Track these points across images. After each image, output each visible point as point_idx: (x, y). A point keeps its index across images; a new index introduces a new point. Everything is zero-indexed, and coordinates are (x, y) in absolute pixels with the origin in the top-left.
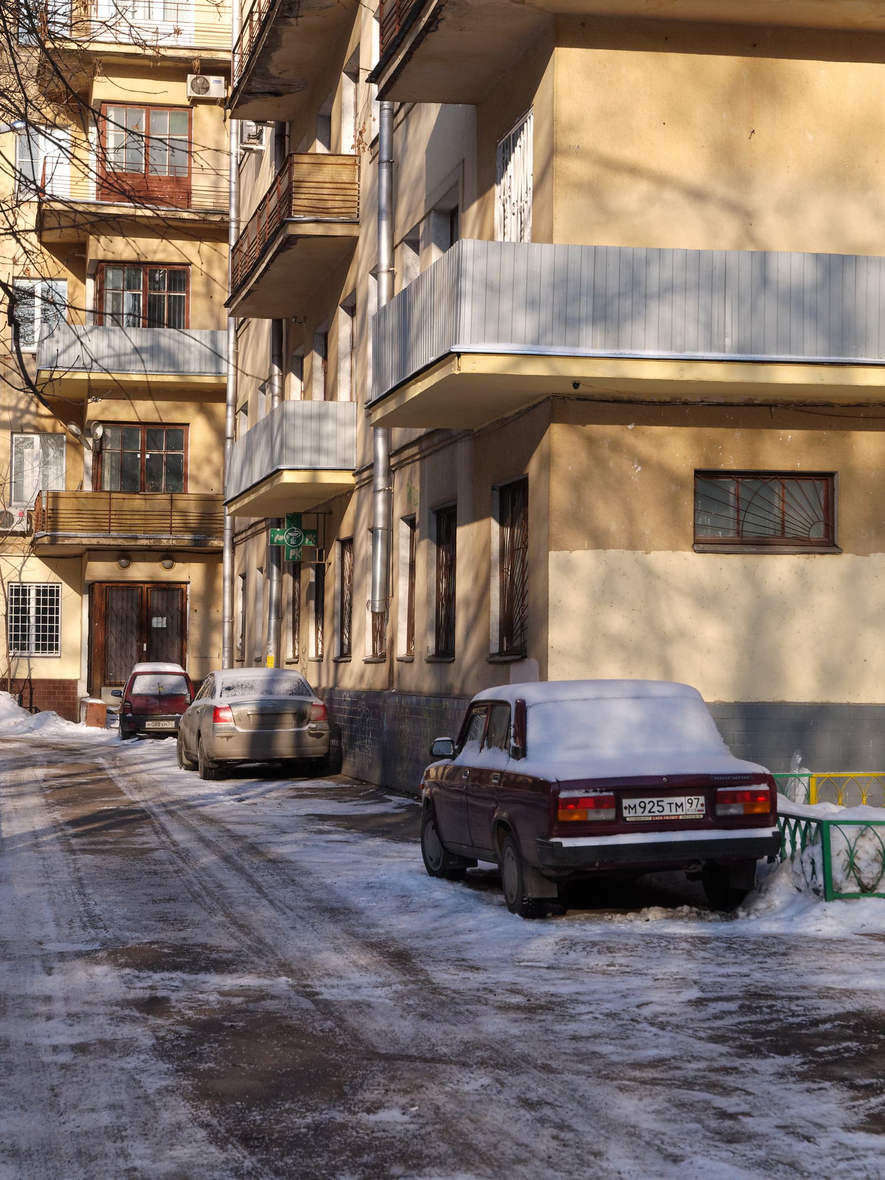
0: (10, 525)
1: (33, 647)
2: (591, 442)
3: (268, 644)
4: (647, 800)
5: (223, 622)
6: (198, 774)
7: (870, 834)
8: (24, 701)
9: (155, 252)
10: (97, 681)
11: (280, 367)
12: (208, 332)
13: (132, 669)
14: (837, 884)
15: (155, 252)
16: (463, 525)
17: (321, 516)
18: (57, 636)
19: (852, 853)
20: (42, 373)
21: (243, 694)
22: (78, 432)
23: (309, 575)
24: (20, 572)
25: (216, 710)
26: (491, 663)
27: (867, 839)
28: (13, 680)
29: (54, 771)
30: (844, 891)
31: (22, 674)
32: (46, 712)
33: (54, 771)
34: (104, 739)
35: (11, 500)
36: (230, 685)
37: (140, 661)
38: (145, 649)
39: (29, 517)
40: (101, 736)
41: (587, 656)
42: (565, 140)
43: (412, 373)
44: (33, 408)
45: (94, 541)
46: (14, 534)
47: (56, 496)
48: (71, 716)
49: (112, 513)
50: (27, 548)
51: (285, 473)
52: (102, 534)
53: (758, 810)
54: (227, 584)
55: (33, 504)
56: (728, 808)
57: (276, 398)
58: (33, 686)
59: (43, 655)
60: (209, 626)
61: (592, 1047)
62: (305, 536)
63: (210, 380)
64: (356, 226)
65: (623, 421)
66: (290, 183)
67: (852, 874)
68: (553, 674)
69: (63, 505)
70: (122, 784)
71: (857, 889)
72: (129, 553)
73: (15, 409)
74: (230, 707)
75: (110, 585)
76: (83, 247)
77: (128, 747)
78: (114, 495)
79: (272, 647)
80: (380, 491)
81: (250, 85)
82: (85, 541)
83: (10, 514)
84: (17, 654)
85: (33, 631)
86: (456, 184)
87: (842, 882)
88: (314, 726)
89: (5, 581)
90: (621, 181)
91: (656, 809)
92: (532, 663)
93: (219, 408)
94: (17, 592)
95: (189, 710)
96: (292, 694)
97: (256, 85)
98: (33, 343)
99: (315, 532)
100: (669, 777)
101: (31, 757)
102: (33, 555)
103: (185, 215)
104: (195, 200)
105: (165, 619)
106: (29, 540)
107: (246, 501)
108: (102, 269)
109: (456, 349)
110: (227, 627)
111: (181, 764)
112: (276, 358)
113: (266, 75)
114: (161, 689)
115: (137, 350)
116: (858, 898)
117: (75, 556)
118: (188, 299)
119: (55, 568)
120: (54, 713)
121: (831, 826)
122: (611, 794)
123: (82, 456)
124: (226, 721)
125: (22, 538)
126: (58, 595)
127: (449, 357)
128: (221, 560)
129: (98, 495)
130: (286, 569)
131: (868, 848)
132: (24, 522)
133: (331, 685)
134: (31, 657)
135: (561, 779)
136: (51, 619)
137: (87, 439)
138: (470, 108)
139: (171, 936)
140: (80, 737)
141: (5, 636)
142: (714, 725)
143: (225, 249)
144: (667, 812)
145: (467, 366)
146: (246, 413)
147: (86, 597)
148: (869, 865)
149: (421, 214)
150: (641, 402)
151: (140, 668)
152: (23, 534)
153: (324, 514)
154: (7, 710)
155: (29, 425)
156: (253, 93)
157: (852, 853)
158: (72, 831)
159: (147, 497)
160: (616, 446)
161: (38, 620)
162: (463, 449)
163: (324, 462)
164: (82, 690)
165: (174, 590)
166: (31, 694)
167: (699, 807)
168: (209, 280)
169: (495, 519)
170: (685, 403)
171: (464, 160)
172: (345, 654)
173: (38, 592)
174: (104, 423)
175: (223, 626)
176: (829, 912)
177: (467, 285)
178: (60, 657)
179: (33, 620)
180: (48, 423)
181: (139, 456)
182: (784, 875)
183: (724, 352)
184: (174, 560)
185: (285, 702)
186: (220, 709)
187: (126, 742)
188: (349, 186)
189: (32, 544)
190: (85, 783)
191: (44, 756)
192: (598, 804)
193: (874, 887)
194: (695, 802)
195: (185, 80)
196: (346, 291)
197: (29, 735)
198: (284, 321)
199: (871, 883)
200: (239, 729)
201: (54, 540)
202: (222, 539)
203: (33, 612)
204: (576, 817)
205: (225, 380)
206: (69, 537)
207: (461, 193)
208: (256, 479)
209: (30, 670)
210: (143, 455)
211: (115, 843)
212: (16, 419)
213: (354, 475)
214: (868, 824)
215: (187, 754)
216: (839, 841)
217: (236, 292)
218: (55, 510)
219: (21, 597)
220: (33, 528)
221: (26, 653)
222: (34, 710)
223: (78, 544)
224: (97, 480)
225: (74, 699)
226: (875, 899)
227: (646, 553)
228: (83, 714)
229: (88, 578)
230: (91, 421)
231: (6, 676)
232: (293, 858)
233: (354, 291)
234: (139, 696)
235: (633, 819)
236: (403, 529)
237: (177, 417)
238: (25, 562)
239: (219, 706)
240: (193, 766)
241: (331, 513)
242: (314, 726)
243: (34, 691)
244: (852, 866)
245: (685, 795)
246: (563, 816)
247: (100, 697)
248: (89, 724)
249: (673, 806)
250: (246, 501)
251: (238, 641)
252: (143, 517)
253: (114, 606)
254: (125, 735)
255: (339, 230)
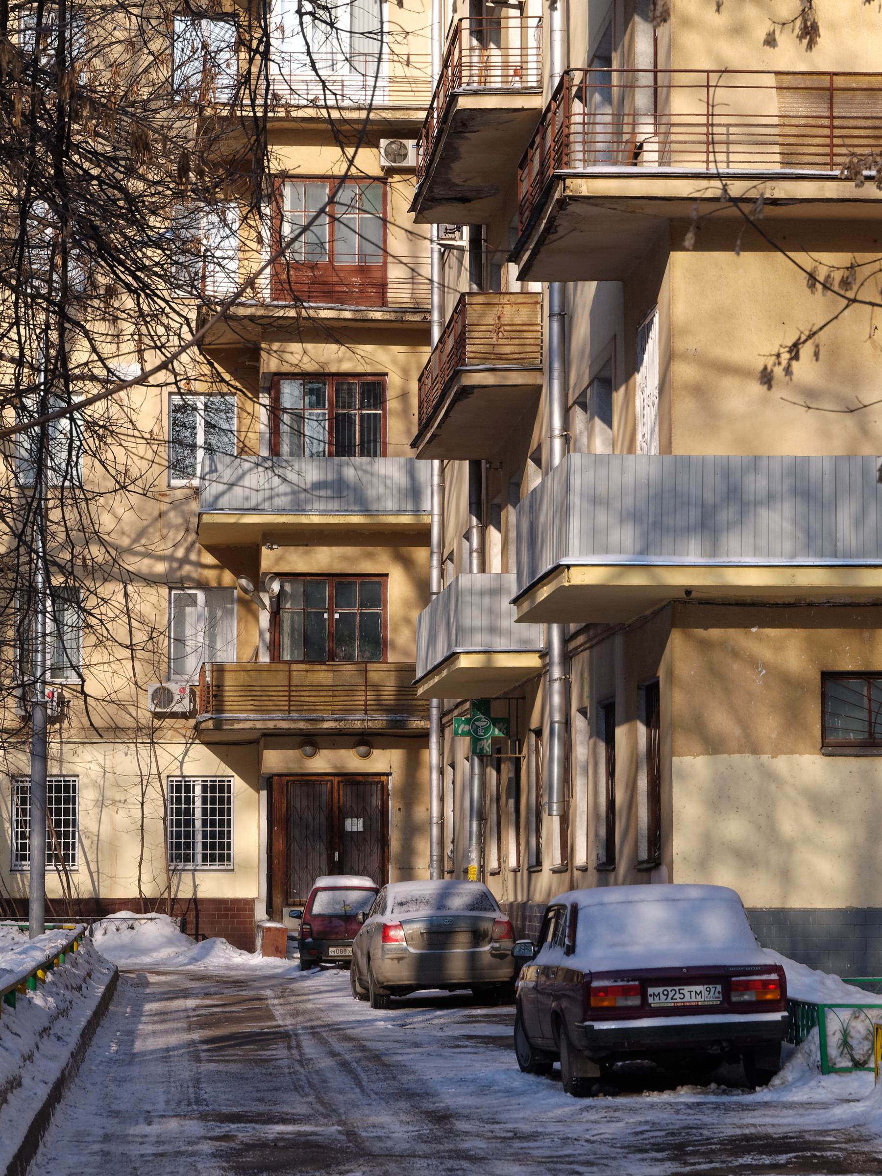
0: (169, 705)
1: (199, 857)
2: (705, 645)
3: (470, 851)
4: (669, 989)
5: (431, 823)
6: (369, 1004)
7: (862, 1016)
8: (188, 926)
9: (340, 361)
10: (278, 900)
11: (479, 518)
12: (402, 460)
13: (314, 881)
14: (831, 1059)
15: (340, 361)
16: (619, 725)
17: (513, 702)
18: (229, 843)
19: (845, 1033)
20: (204, 516)
21: (417, 910)
22: (251, 587)
23: (507, 770)
24: (182, 763)
25: (385, 928)
26: (639, 870)
27: (859, 1020)
28: (175, 901)
29: (208, 1002)
30: (838, 1066)
31: (185, 892)
32: (214, 939)
33: (208, 1002)
34: (279, 971)
35: (169, 673)
36: (404, 900)
37: (321, 874)
38: (337, 859)
39: (193, 693)
40: (276, 967)
41: (703, 863)
42: (680, 345)
43: (539, 576)
44: (193, 557)
45: (271, 725)
46: (174, 715)
47: (219, 670)
48: (245, 944)
49: (293, 688)
50: (189, 733)
51: (462, 656)
52: (279, 715)
53: (769, 997)
54: (435, 776)
55: (197, 677)
56: (743, 995)
57: (475, 555)
58: (199, 907)
59: (212, 867)
60: (411, 830)
61: (527, 1151)
62: (494, 726)
63: (406, 519)
64: (538, 374)
65: (745, 624)
66: (464, 326)
67: (846, 1051)
68: (678, 879)
69: (229, 680)
70: (278, 1012)
71: (850, 1064)
72: (314, 738)
73: (171, 558)
74: (401, 925)
75: (291, 778)
76: (255, 353)
77: (304, 978)
78: (294, 667)
79: (474, 855)
80: (556, 680)
81: (432, 192)
82: (259, 725)
83: (169, 690)
84: (180, 867)
85: (199, 838)
86: (610, 358)
87: (836, 1057)
88: (497, 945)
89: (163, 776)
90: (729, 383)
91: (677, 996)
92: (664, 869)
93: (420, 554)
94: (178, 789)
95: (363, 929)
96: (473, 909)
97: (439, 192)
98: (194, 475)
99: (506, 721)
100: (688, 968)
101: (187, 989)
102: (197, 741)
103: (378, 315)
104: (391, 295)
105: (361, 820)
106: (192, 722)
107: (431, 683)
108: (278, 384)
109: (565, 561)
110: (435, 830)
111: (356, 994)
112: (474, 506)
113: (448, 184)
114: (348, 908)
115: (318, 485)
116: (851, 1072)
117: (250, 742)
118: (385, 418)
119: (226, 759)
120: (224, 940)
121: (826, 1009)
122: (637, 983)
123: (257, 620)
124: (397, 941)
125: (183, 721)
126: (229, 792)
127: (558, 569)
128: (427, 746)
129: (274, 666)
130: (489, 763)
131: (860, 1028)
132: (186, 701)
133: (525, 899)
134: (196, 870)
135: (593, 970)
136: (222, 822)
137: (261, 595)
138: (612, 286)
139: (261, 1108)
140: (254, 968)
141: (163, 845)
142: (747, 924)
143: (425, 353)
144: (687, 999)
145: (577, 578)
146: (452, 560)
147: (264, 793)
148: (860, 1043)
149: (586, 381)
150: (763, 605)
151: (323, 882)
152: (184, 716)
153: (517, 699)
154: (166, 937)
155: (188, 578)
156: (437, 200)
157: (845, 1033)
158: (205, 1047)
159: (335, 668)
160: (735, 654)
161: (204, 823)
162: (619, 641)
163: (500, 643)
164: (260, 913)
165: (366, 783)
166: (197, 917)
167: (716, 994)
168: (404, 396)
169: (642, 721)
170: (810, 605)
171: (615, 335)
172: (536, 865)
173: (205, 789)
174: (282, 576)
175: (431, 829)
176: (823, 1083)
177: (575, 500)
178: (233, 870)
179: (198, 824)
180: (211, 575)
181: (326, 616)
182: (799, 1055)
183: (836, 556)
184: (371, 746)
185: (457, 917)
186: (390, 927)
187: (305, 973)
188: (525, 328)
189: (196, 727)
190: (238, 1012)
191: (203, 988)
192: (626, 992)
193: (865, 1062)
194: (713, 990)
195: (377, 146)
196: (534, 445)
197: (189, 967)
198: (483, 462)
199: (863, 1059)
200: (412, 950)
201: (219, 724)
202: (427, 717)
203: (198, 813)
204: (606, 1004)
205: (426, 520)
206: (239, 720)
207: (613, 367)
208: (439, 659)
209: (195, 887)
210: (331, 615)
211: (243, 1055)
212: (171, 570)
213: (540, 657)
214: (860, 1008)
215: (360, 980)
216: (834, 1023)
217: (424, 427)
218: (220, 687)
219: (183, 795)
220: (198, 707)
221: (190, 866)
222: (200, 937)
223: (251, 729)
224: (274, 648)
225: (252, 922)
226: (866, 1072)
227: (772, 757)
228: (259, 942)
229: (264, 770)
230: (266, 574)
231: (166, 896)
232: (408, 1064)
233: (539, 446)
234: (319, 916)
235: (658, 1005)
236: (580, 723)
237: (368, 567)
238: (187, 751)
239: (389, 924)
240: (364, 997)
241: (524, 698)
242: (497, 945)
243: (201, 913)
244: (845, 1043)
245: (703, 984)
246: (594, 1002)
247: (281, 920)
248: (265, 954)
249: (693, 994)
250: (431, 683)
251: (449, 847)
252: (330, 693)
253: (298, 806)
254: (306, 965)
255: (517, 379)
